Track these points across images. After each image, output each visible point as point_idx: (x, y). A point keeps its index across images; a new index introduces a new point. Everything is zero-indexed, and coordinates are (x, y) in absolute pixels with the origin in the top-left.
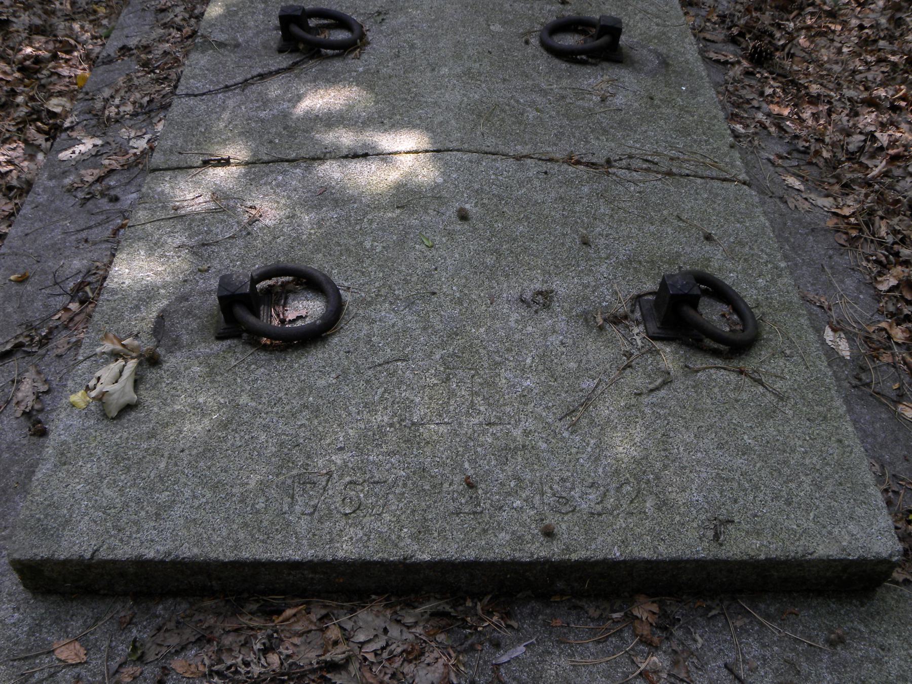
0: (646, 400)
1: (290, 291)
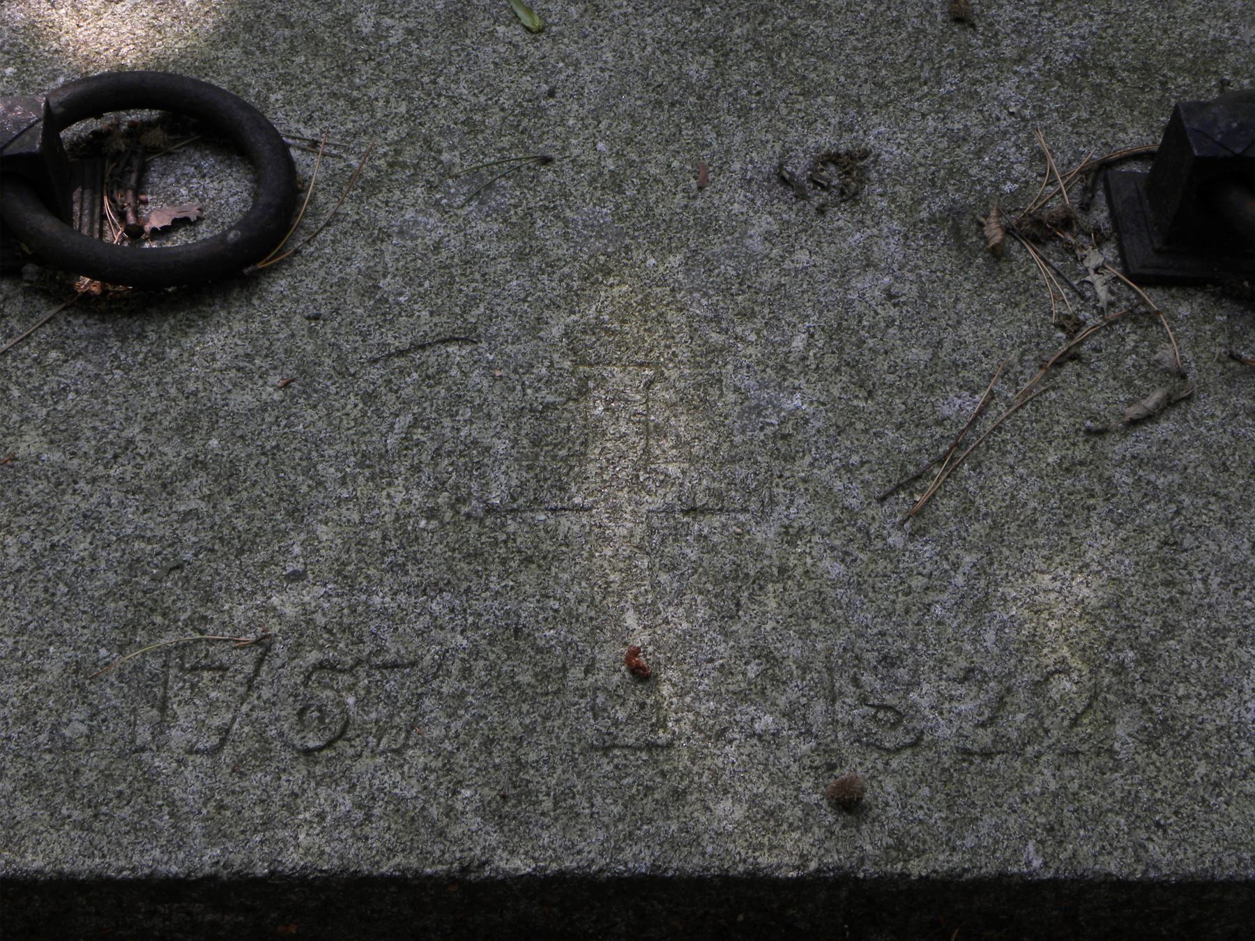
0: (1117, 447)
1: (155, 150)
